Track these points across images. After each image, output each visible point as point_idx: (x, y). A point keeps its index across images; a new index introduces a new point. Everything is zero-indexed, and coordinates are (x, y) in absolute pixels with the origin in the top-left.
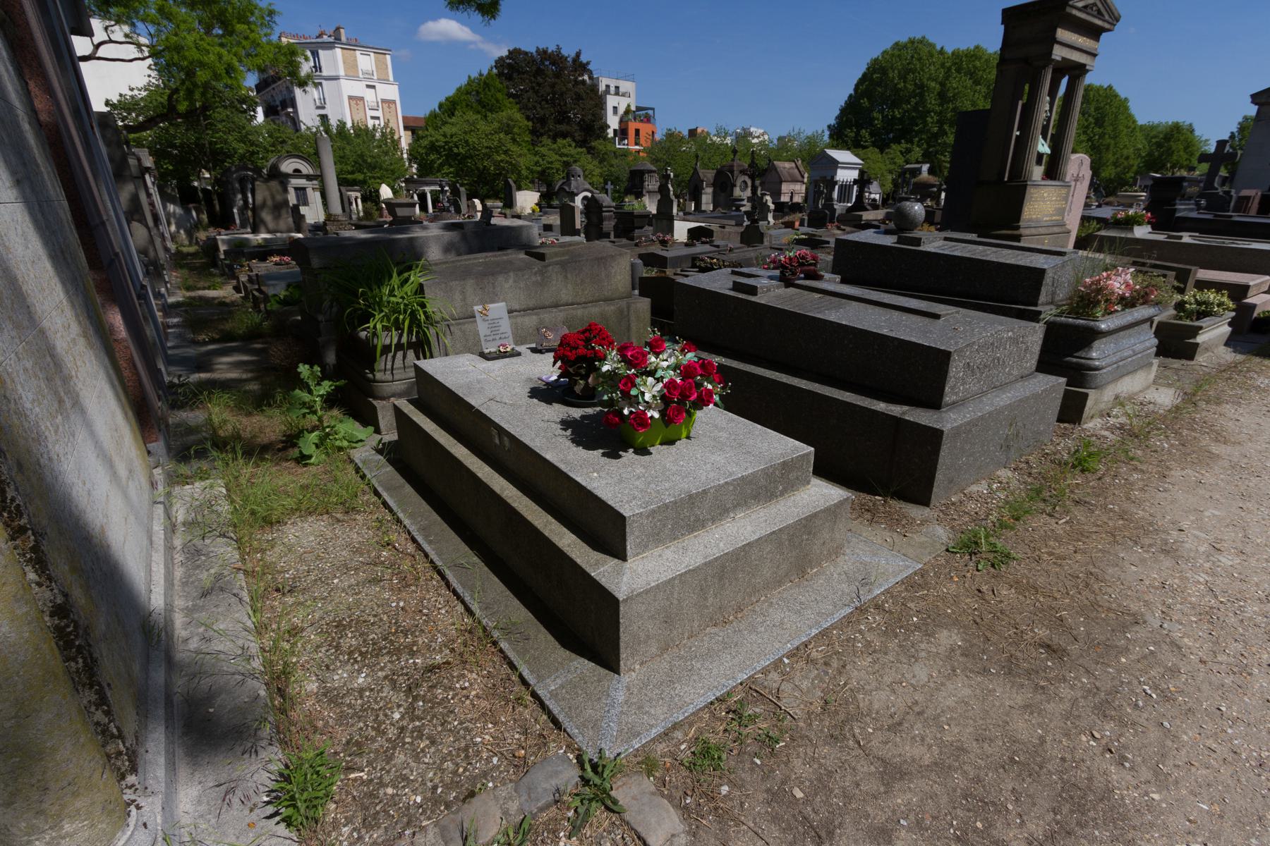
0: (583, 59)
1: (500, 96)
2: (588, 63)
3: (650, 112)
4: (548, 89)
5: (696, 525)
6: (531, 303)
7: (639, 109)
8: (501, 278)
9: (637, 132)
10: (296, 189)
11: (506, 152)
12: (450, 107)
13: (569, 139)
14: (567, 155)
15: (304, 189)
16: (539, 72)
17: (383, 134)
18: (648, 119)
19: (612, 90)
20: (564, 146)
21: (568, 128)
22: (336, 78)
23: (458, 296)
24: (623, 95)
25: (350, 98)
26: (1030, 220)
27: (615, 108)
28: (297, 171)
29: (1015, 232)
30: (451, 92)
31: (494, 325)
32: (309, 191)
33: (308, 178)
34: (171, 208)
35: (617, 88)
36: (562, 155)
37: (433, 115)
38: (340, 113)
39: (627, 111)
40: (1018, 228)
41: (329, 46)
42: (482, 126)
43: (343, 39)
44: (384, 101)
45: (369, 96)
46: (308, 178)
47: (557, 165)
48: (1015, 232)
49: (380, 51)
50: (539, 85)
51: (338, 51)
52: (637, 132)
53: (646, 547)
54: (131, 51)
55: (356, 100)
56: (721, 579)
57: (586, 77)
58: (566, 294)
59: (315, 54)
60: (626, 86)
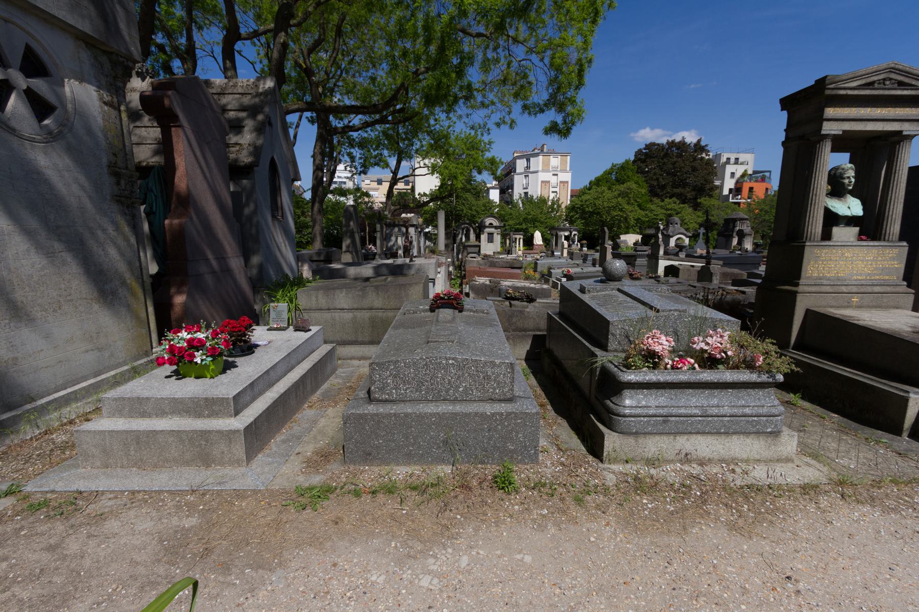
0: (703, 143)
1: (630, 173)
2: (706, 145)
3: (767, 174)
4: (671, 166)
5: (144, 415)
6: (355, 306)
7: (755, 172)
8: (338, 292)
9: (751, 189)
10: (489, 234)
11: (621, 210)
12: (598, 182)
13: (674, 199)
14: (671, 209)
15: (492, 234)
16: (666, 155)
17: (553, 203)
18: (763, 179)
19: (732, 161)
20: (670, 204)
21: (682, 191)
22: (537, 172)
23: (314, 298)
24: (742, 164)
25: (542, 182)
26: (809, 278)
27: (733, 174)
28: (491, 224)
29: (794, 289)
30: (599, 173)
31: (279, 314)
32: (495, 235)
33: (496, 228)
34: (428, 243)
35: (737, 159)
36: (667, 210)
37: (585, 188)
38: (536, 192)
39: (743, 175)
40: (797, 285)
41: (537, 155)
42: (608, 194)
43: (545, 150)
44: (561, 182)
45: (553, 180)
46: (496, 228)
47: (661, 217)
48: (794, 289)
49: (564, 155)
50: (664, 163)
51: (541, 157)
52: (751, 189)
53: (113, 416)
54: (425, 171)
55: (546, 183)
56: (138, 443)
57: (704, 155)
58: (378, 303)
59: (528, 160)
60: (743, 157)
